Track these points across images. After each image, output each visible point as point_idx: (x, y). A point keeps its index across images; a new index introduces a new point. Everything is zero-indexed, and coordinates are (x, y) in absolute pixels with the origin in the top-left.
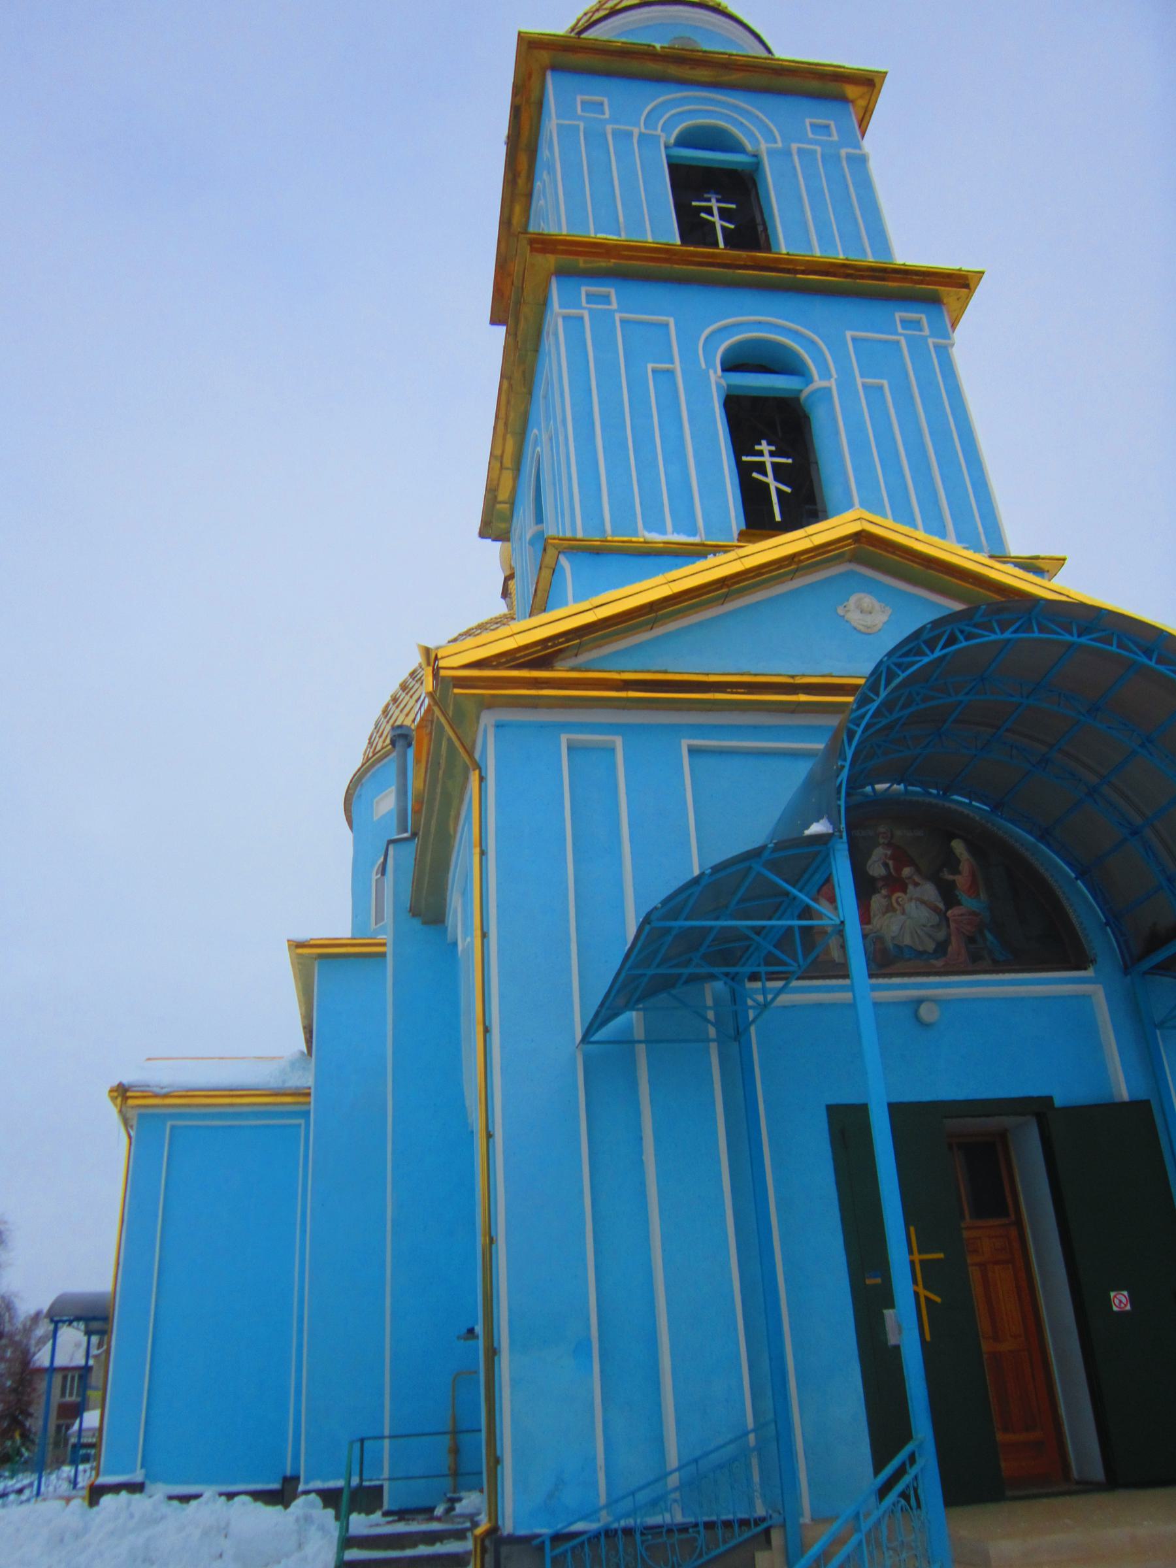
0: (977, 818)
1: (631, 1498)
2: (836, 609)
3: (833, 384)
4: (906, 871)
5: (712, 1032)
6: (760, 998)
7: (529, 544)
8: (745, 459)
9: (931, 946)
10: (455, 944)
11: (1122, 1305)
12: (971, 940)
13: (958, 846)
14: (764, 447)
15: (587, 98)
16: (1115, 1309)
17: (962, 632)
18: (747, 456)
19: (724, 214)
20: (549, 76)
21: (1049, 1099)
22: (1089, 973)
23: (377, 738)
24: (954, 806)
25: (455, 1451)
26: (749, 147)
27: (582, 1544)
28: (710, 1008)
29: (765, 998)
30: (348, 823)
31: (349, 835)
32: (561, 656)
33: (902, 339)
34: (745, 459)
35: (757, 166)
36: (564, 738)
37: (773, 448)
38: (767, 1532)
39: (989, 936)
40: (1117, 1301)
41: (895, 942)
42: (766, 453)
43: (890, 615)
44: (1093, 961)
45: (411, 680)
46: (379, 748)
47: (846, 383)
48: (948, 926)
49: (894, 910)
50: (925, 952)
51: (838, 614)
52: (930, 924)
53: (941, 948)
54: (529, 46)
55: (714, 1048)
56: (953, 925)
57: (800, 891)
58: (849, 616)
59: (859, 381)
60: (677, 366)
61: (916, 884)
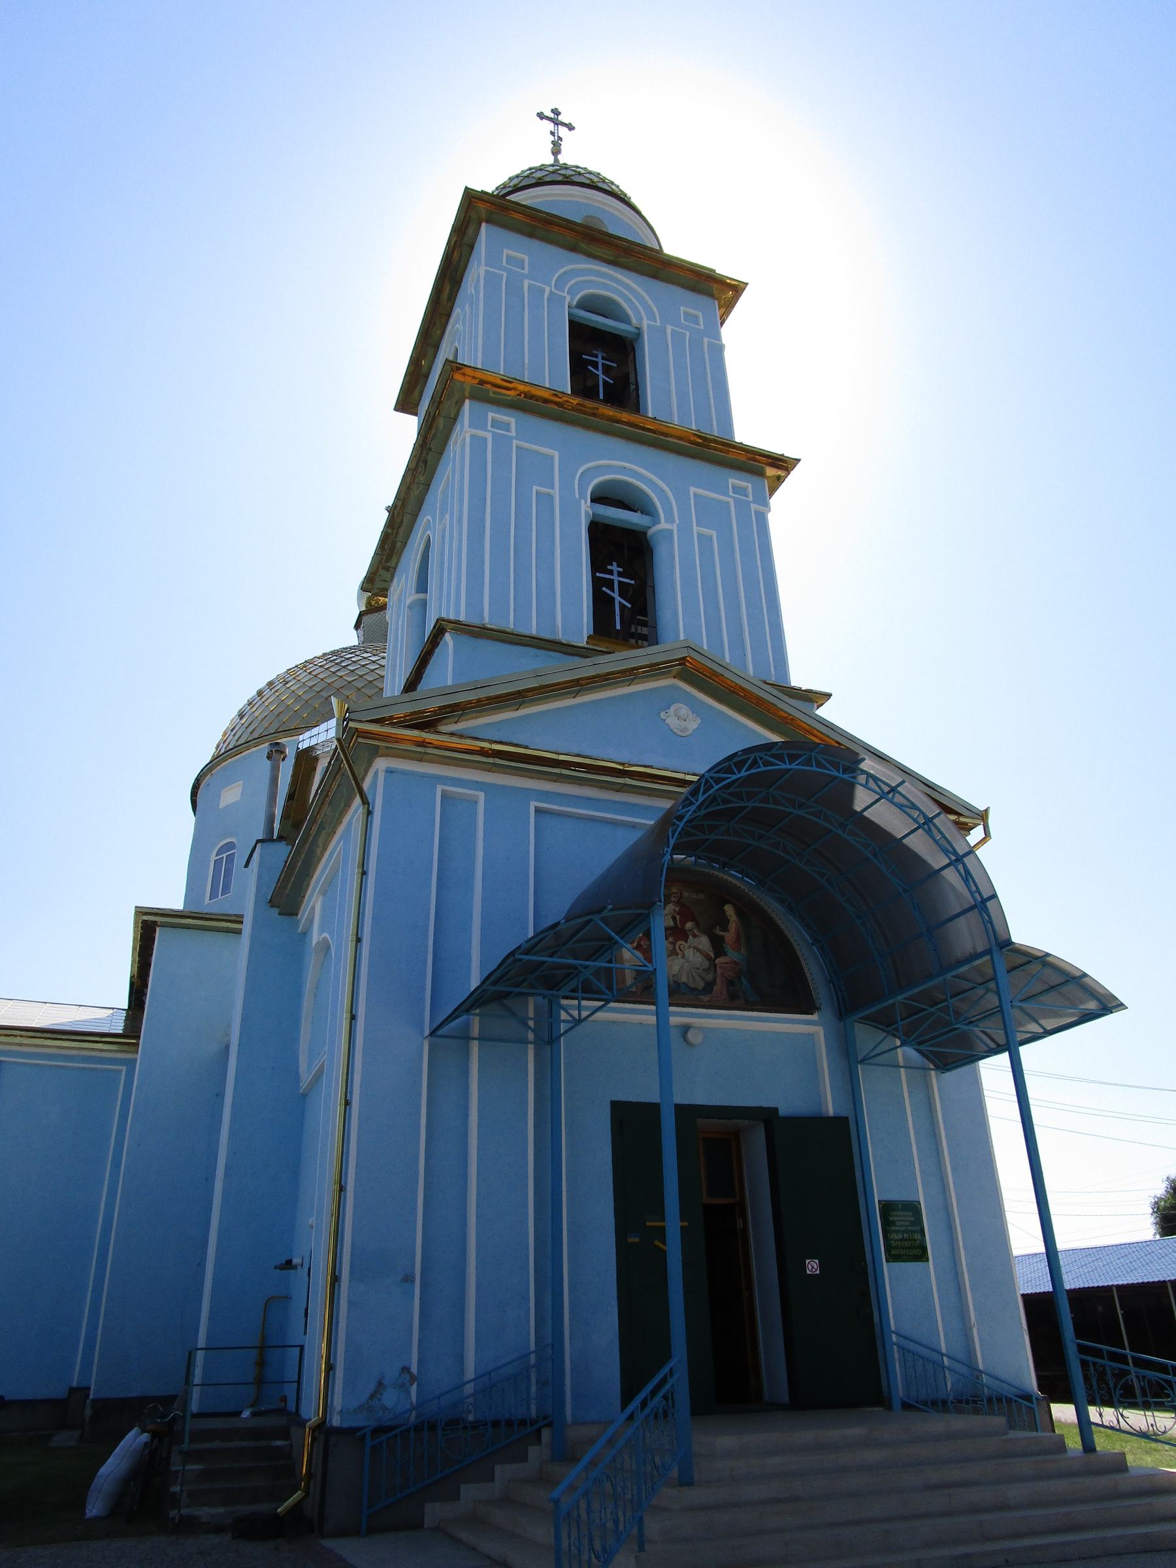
0: (746, 890)
1: (437, 1400)
2: (660, 713)
3: (674, 527)
4: (689, 925)
5: (531, 1036)
6: (575, 1013)
7: (408, 608)
8: (598, 574)
9: (701, 985)
10: (306, 933)
11: (814, 1270)
12: (730, 983)
13: (729, 910)
14: (614, 567)
15: (511, 253)
16: (808, 1272)
17: (761, 758)
18: (600, 573)
19: (607, 370)
20: (484, 225)
21: (776, 1110)
22: (814, 1017)
23: (231, 737)
24: (730, 879)
25: (261, 1363)
26: (634, 321)
27: (396, 1436)
28: (531, 1019)
29: (580, 1014)
30: (192, 806)
31: (190, 819)
32: (444, 721)
33: (731, 501)
34: (598, 574)
35: (639, 334)
36: (439, 788)
37: (621, 570)
38: (539, 1431)
39: (744, 981)
40: (810, 1267)
41: (675, 979)
42: (615, 573)
43: (699, 724)
44: (818, 1009)
45: (269, 690)
46: (231, 746)
47: (685, 529)
48: (715, 970)
49: (677, 954)
50: (695, 989)
51: (660, 717)
52: (702, 968)
53: (709, 987)
54: (471, 199)
55: (531, 1048)
56: (719, 971)
57: (622, 938)
58: (668, 721)
59: (695, 529)
60: (556, 493)
61: (695, 936)
